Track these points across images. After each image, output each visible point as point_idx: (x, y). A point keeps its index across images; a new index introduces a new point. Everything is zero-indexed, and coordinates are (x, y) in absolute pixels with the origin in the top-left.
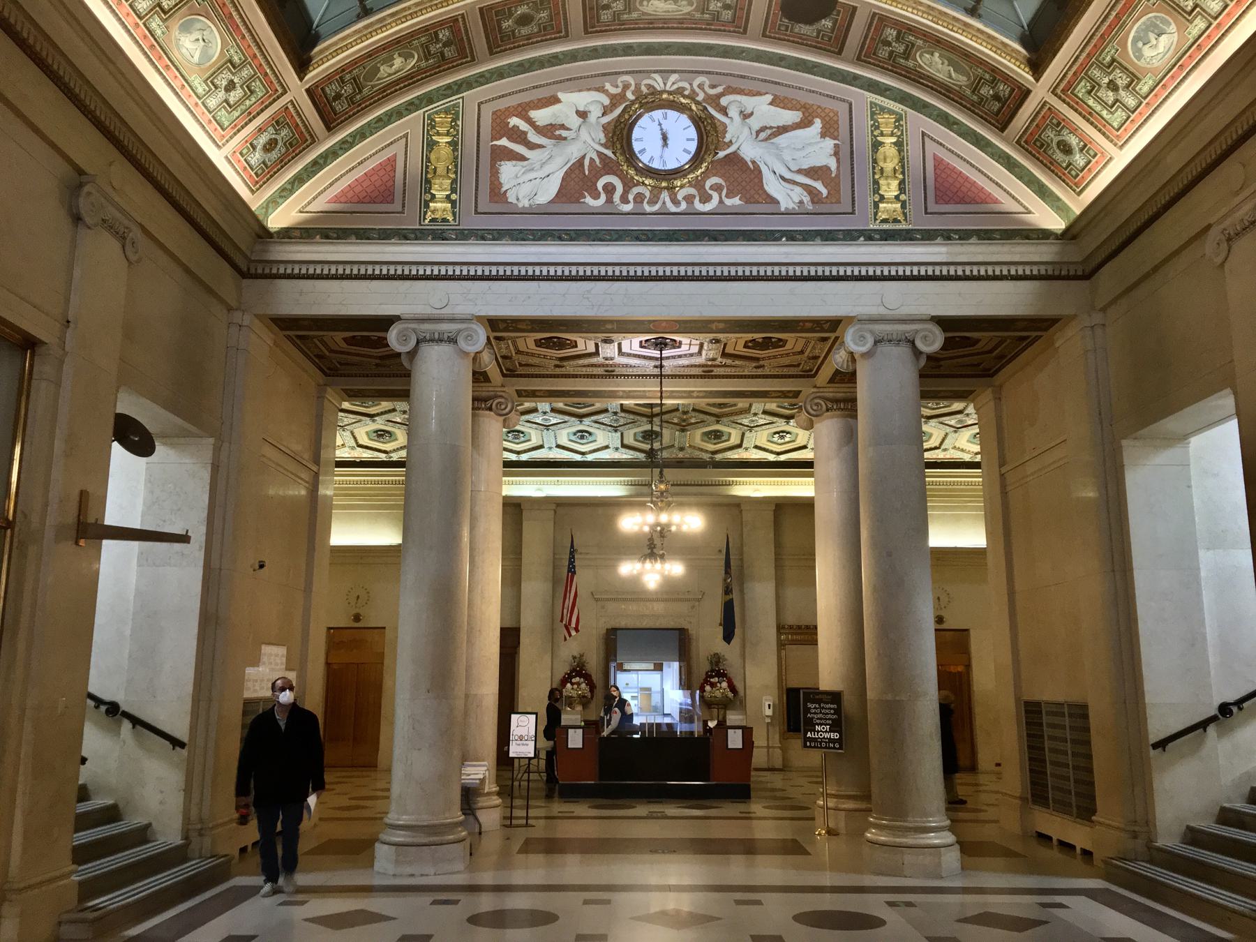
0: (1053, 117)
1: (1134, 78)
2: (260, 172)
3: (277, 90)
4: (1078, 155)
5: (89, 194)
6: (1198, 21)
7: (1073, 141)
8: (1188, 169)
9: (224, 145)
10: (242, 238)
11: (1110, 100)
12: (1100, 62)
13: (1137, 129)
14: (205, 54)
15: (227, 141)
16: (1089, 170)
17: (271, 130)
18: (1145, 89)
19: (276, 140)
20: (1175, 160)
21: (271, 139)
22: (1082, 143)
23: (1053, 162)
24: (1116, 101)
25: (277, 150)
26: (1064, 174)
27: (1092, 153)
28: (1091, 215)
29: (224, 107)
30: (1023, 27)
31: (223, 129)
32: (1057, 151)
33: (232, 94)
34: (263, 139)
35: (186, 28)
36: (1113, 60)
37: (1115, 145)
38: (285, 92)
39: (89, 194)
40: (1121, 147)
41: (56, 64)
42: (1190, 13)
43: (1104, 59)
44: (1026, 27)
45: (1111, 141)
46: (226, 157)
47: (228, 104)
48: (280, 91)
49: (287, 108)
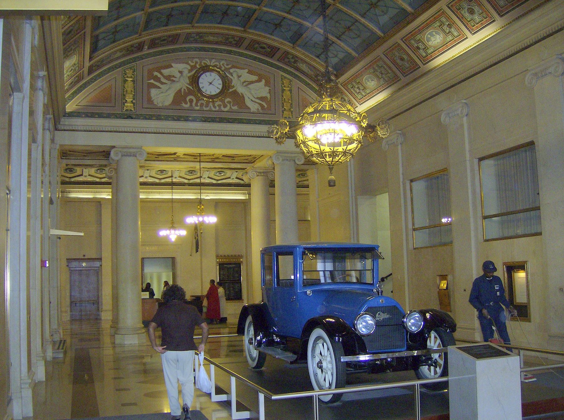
6: (450, 36)
18: (368, 92)
23: (463, 17)
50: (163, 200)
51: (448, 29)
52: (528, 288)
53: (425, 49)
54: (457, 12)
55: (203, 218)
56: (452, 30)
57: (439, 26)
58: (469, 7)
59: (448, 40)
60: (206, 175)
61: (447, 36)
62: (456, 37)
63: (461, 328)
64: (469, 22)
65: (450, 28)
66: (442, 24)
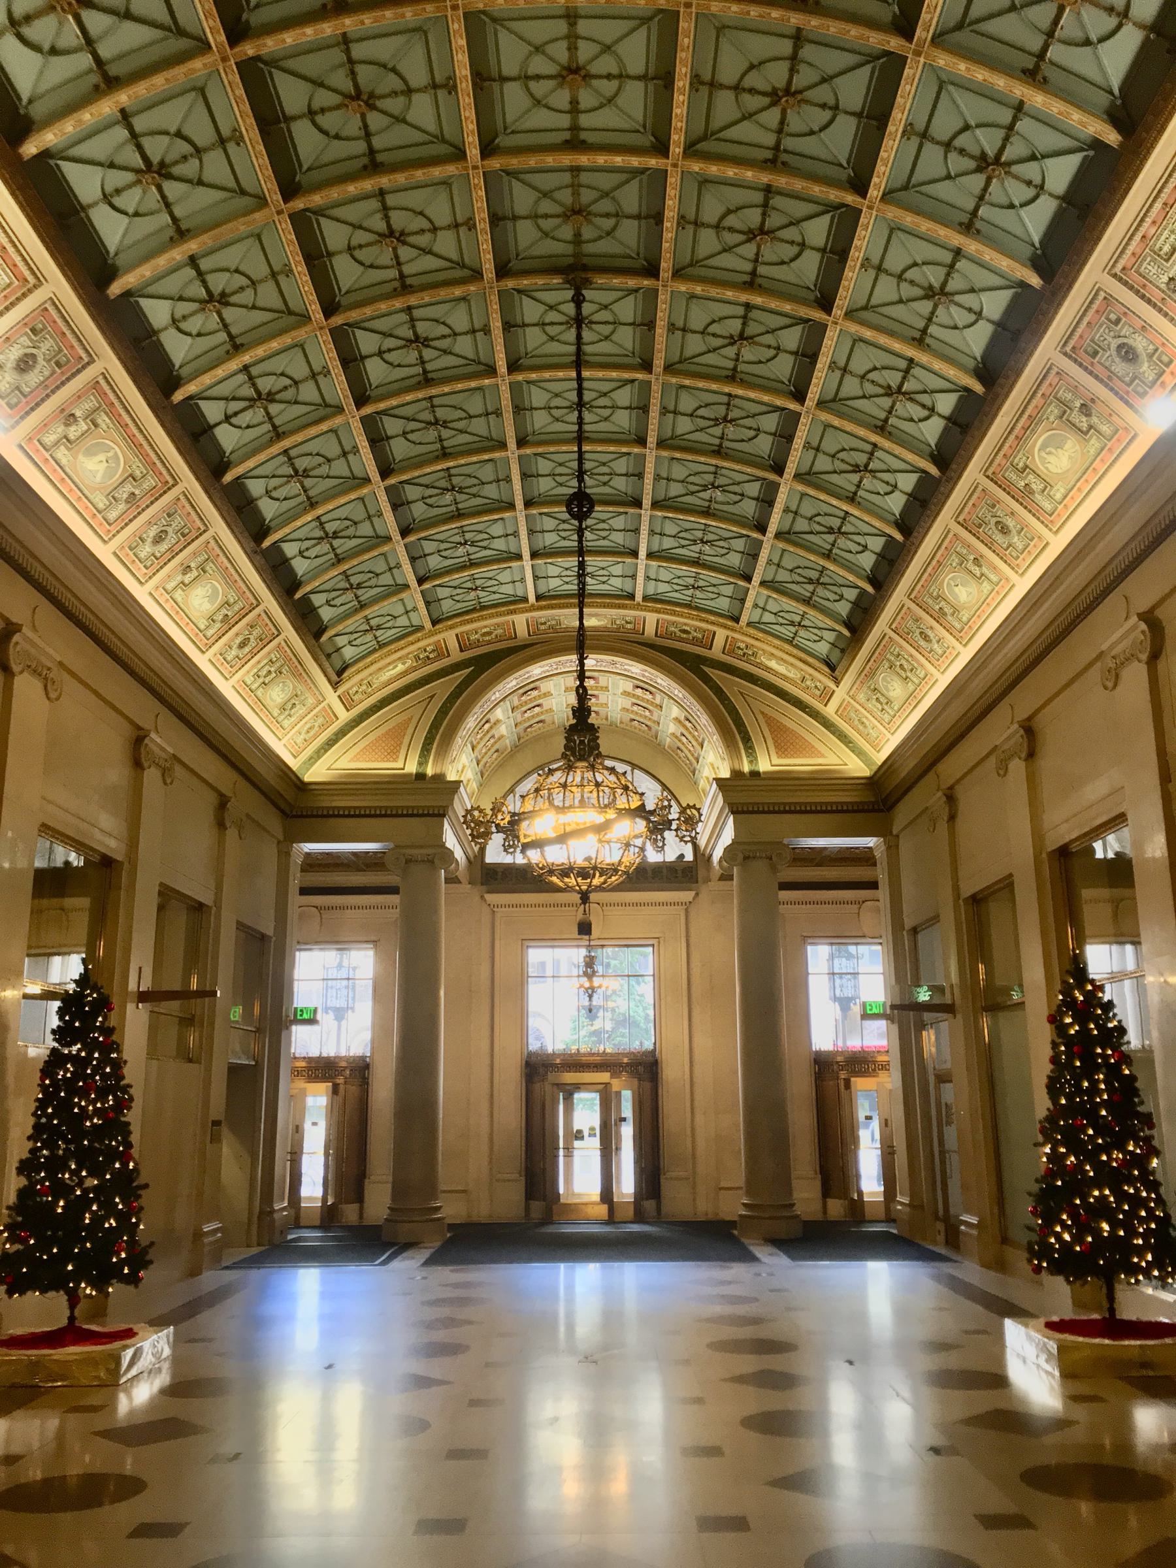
0: (1111, 311)
1: (1047, 485)
2: (149, 564)
3: (26, 280)
4: (1146, 364)
5: (17, 643)
6: (1093, 441)
7: (1139, 343)
8: (1083, 597)
9: (110, 539)
10: (289, 795)
11: (1084, 426)
12: (1155, 253)
13: (1091, 489)
14: (110, 473)
15: (114, 536)
16: (1079, 490)
17: (25, 340)
18: (1058, 496)
19: (33, 356)
20: (977, 687)
21: (26, 355)
22: (1151, 347)
23: (1112, 374)
24: (1091, 427)
25: (36, 371)
26: (1127, 393)
27: (1165, 359)
28: (889, 762)
29: (64, 444)
30: (1033, 245)
31: (110, 524)
32: (1117, 360)
33: (73, 428)
34: (153, 532)
35: (90, 453)
36: (1026, 467)
37: (1050, 530)
38: (175, 484)
39: (17, 643)
40: (965, 645)
41: (36, 570)
42: (1086, 433)
43: (1161, 249)
44: (1037, 245)
45: (1047, 526)
46: (115, 554)
47: (68, 440)
48: (171, 482)
49: (46, 309)
50: (239, 536)
51: (1084, 419)
52: (320, 865)
53: (956, 611)
54: (1092, 364)
55: (294, 118)
56: (1095, 420)
57: (1061, 417)
58: (1120, 341)
59: (986, 592)
60: (912, 71)
61: (1087, 441)
62: (1109, 440)
63: (241, 334)
64: (1129, 385)
65: (1086, 415)
66: (963, 559)
